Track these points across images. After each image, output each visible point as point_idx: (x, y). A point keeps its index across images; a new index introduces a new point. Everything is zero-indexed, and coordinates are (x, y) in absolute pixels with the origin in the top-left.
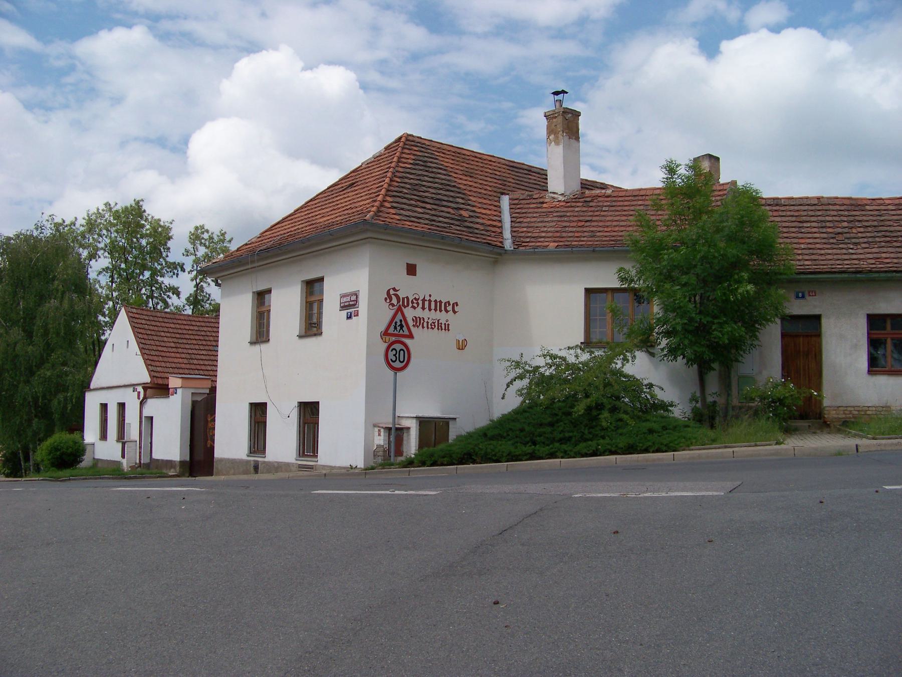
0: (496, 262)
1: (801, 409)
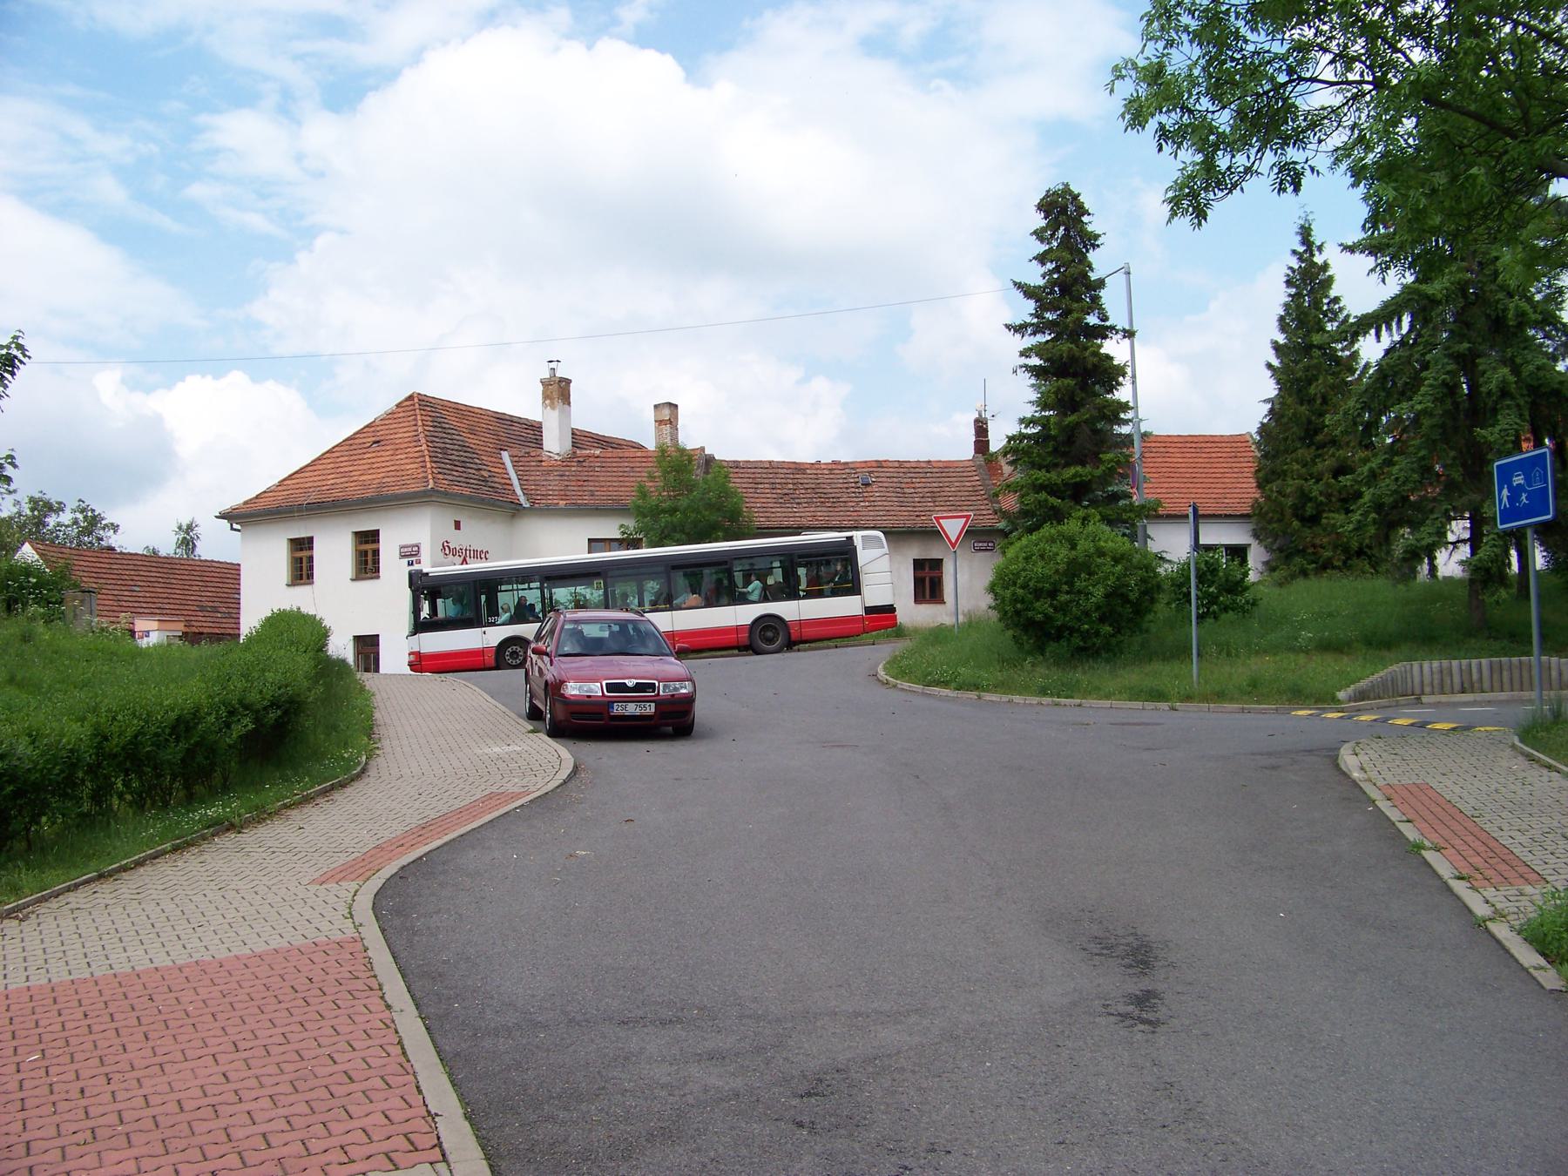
0: (513, 516)
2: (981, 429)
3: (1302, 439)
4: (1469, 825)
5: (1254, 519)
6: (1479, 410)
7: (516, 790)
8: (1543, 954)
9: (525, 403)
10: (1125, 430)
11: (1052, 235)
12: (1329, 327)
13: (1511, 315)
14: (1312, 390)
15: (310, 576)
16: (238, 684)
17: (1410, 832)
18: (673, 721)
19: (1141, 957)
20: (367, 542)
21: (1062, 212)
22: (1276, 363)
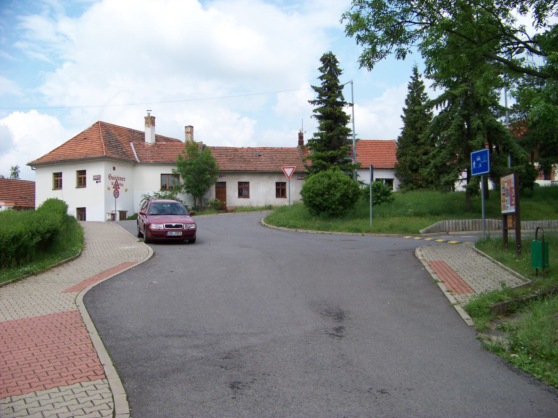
0: (134, 166)
1: (221, 207)
2: (301, 137)
3: (412, 142)
4: (454, 274)
5: (395, 170)
6: (470, 134)
7: (133, 261)
8: (470, 315)
9: (139, 125)
10: (350, 138)
11: (325, 70)
12: (423, 103)
13: (481, 102)
14: (416, 125)
15: (61, 186)
16: (35, 224)
17: (434, 277)
18: (188, 238)
19: (340, 316)
20: (82, 174)
21: (329, 62)
22: (404, 116)
